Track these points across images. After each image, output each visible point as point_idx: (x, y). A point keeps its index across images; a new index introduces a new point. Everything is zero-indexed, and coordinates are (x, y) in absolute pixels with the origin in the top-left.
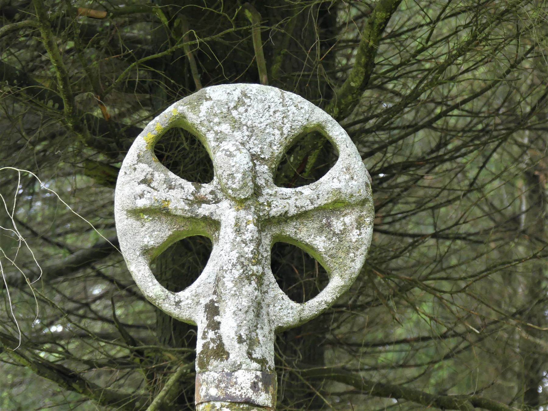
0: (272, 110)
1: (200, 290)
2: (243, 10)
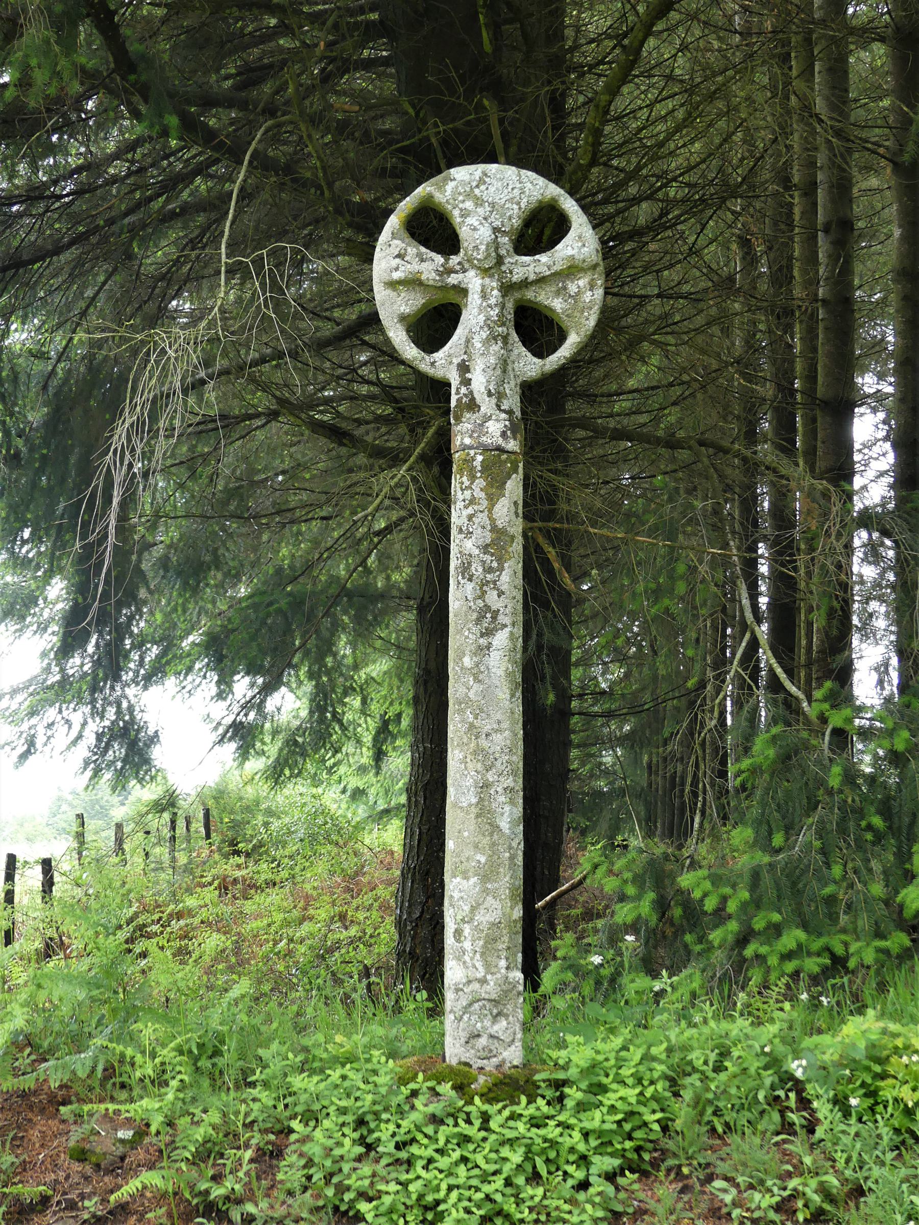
0: (510, 187)
1: (452, 351)
2: (481, 100)
